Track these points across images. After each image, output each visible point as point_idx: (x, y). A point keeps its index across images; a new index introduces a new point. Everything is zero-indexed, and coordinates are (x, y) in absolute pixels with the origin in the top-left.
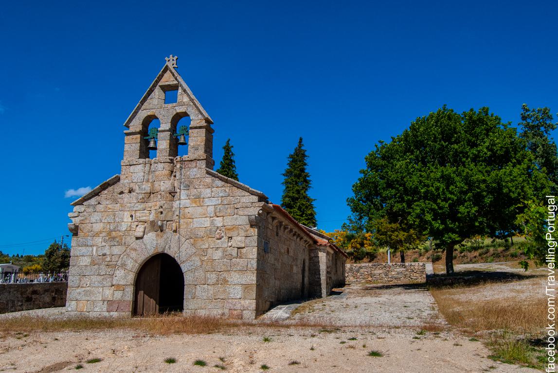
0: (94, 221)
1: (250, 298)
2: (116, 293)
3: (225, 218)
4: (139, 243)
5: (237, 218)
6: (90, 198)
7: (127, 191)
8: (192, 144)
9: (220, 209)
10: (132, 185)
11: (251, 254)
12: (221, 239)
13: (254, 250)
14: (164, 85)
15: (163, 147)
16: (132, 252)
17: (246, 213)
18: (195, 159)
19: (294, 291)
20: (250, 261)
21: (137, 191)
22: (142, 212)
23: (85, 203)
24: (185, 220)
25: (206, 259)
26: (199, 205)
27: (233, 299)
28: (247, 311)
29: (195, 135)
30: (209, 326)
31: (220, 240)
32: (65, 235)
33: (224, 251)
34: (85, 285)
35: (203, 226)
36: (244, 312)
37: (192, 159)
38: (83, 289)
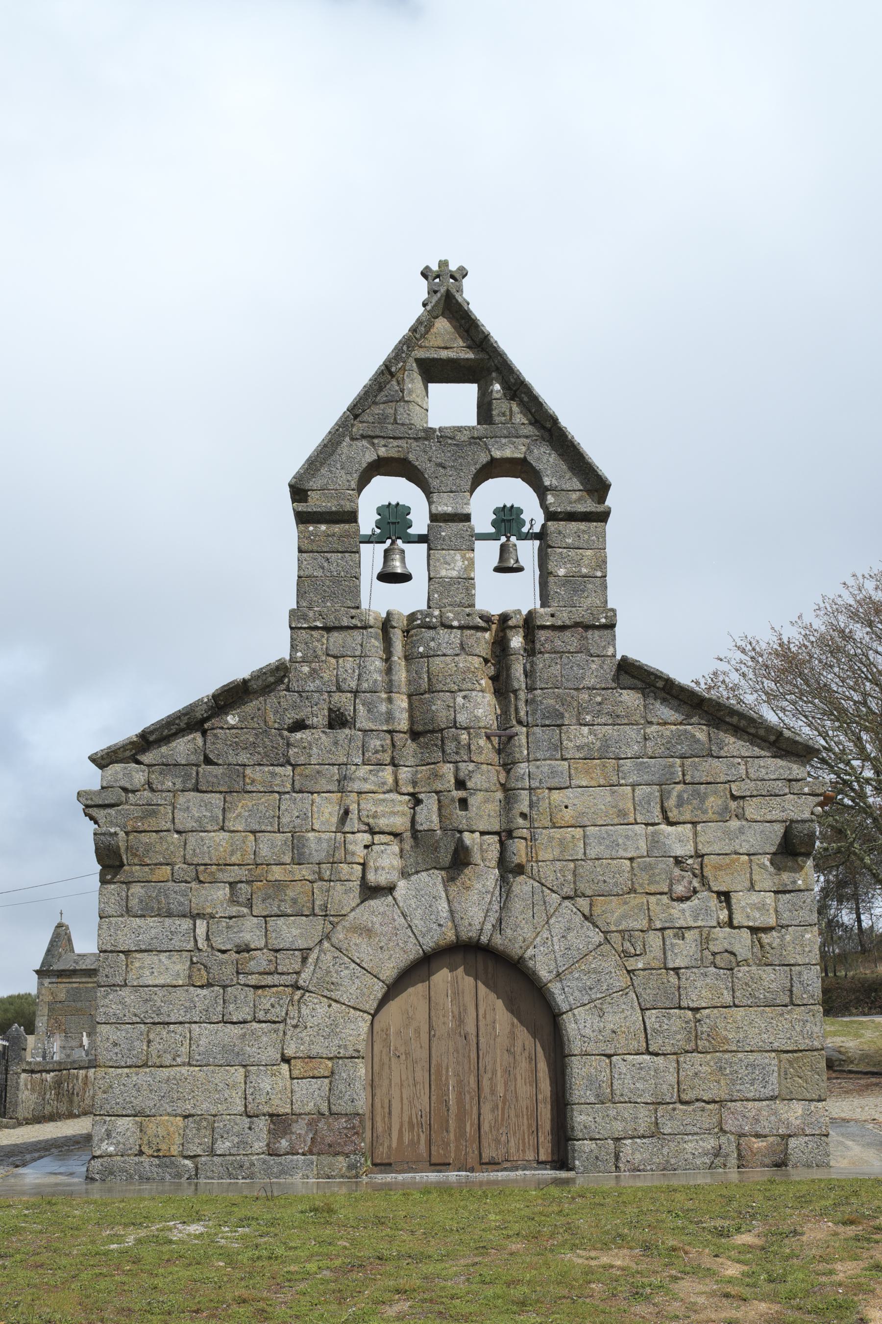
0: (191, 824)
1: (808, 1096)
2: (302, 1088)
3: (699, 827)
4: (382, 910)
5: (741, 831)
6: (165, 739)
7: (320, 719)
8: (562, 572)
9: (679, 797)
10: (343, 701)
11: (799, 948)
12: (688, 899)
13: (808, 936)
14: (434, 359)
15: (454, 574)
16: (356, 939)
17: (776, 815)
18: (577, 625)
19: (866, 1010)
20: (800, 973)
21: (363, 722)
22: (382, 796)
23: (147, 758)
24: (556, 833)
25: (640, 966)
26: (602, 782)
27: (748, 1100)
28: (803, 1139)
29: (569, 541)
30: (446, 891)
31: (688, 903)
32: (97, 1184)
33: (705, 940)
34: (167, 1059)
35: (622, 853)
36: (792, 1143)
37: (568, 623)
38: (165, 1073)
